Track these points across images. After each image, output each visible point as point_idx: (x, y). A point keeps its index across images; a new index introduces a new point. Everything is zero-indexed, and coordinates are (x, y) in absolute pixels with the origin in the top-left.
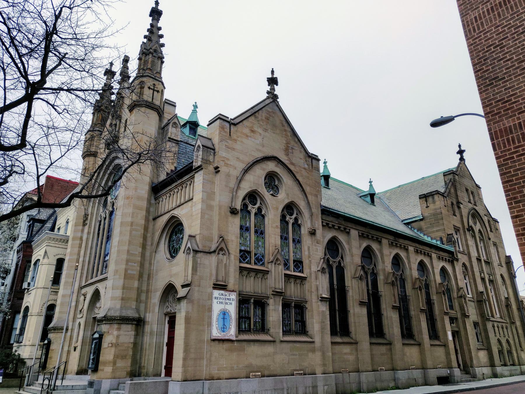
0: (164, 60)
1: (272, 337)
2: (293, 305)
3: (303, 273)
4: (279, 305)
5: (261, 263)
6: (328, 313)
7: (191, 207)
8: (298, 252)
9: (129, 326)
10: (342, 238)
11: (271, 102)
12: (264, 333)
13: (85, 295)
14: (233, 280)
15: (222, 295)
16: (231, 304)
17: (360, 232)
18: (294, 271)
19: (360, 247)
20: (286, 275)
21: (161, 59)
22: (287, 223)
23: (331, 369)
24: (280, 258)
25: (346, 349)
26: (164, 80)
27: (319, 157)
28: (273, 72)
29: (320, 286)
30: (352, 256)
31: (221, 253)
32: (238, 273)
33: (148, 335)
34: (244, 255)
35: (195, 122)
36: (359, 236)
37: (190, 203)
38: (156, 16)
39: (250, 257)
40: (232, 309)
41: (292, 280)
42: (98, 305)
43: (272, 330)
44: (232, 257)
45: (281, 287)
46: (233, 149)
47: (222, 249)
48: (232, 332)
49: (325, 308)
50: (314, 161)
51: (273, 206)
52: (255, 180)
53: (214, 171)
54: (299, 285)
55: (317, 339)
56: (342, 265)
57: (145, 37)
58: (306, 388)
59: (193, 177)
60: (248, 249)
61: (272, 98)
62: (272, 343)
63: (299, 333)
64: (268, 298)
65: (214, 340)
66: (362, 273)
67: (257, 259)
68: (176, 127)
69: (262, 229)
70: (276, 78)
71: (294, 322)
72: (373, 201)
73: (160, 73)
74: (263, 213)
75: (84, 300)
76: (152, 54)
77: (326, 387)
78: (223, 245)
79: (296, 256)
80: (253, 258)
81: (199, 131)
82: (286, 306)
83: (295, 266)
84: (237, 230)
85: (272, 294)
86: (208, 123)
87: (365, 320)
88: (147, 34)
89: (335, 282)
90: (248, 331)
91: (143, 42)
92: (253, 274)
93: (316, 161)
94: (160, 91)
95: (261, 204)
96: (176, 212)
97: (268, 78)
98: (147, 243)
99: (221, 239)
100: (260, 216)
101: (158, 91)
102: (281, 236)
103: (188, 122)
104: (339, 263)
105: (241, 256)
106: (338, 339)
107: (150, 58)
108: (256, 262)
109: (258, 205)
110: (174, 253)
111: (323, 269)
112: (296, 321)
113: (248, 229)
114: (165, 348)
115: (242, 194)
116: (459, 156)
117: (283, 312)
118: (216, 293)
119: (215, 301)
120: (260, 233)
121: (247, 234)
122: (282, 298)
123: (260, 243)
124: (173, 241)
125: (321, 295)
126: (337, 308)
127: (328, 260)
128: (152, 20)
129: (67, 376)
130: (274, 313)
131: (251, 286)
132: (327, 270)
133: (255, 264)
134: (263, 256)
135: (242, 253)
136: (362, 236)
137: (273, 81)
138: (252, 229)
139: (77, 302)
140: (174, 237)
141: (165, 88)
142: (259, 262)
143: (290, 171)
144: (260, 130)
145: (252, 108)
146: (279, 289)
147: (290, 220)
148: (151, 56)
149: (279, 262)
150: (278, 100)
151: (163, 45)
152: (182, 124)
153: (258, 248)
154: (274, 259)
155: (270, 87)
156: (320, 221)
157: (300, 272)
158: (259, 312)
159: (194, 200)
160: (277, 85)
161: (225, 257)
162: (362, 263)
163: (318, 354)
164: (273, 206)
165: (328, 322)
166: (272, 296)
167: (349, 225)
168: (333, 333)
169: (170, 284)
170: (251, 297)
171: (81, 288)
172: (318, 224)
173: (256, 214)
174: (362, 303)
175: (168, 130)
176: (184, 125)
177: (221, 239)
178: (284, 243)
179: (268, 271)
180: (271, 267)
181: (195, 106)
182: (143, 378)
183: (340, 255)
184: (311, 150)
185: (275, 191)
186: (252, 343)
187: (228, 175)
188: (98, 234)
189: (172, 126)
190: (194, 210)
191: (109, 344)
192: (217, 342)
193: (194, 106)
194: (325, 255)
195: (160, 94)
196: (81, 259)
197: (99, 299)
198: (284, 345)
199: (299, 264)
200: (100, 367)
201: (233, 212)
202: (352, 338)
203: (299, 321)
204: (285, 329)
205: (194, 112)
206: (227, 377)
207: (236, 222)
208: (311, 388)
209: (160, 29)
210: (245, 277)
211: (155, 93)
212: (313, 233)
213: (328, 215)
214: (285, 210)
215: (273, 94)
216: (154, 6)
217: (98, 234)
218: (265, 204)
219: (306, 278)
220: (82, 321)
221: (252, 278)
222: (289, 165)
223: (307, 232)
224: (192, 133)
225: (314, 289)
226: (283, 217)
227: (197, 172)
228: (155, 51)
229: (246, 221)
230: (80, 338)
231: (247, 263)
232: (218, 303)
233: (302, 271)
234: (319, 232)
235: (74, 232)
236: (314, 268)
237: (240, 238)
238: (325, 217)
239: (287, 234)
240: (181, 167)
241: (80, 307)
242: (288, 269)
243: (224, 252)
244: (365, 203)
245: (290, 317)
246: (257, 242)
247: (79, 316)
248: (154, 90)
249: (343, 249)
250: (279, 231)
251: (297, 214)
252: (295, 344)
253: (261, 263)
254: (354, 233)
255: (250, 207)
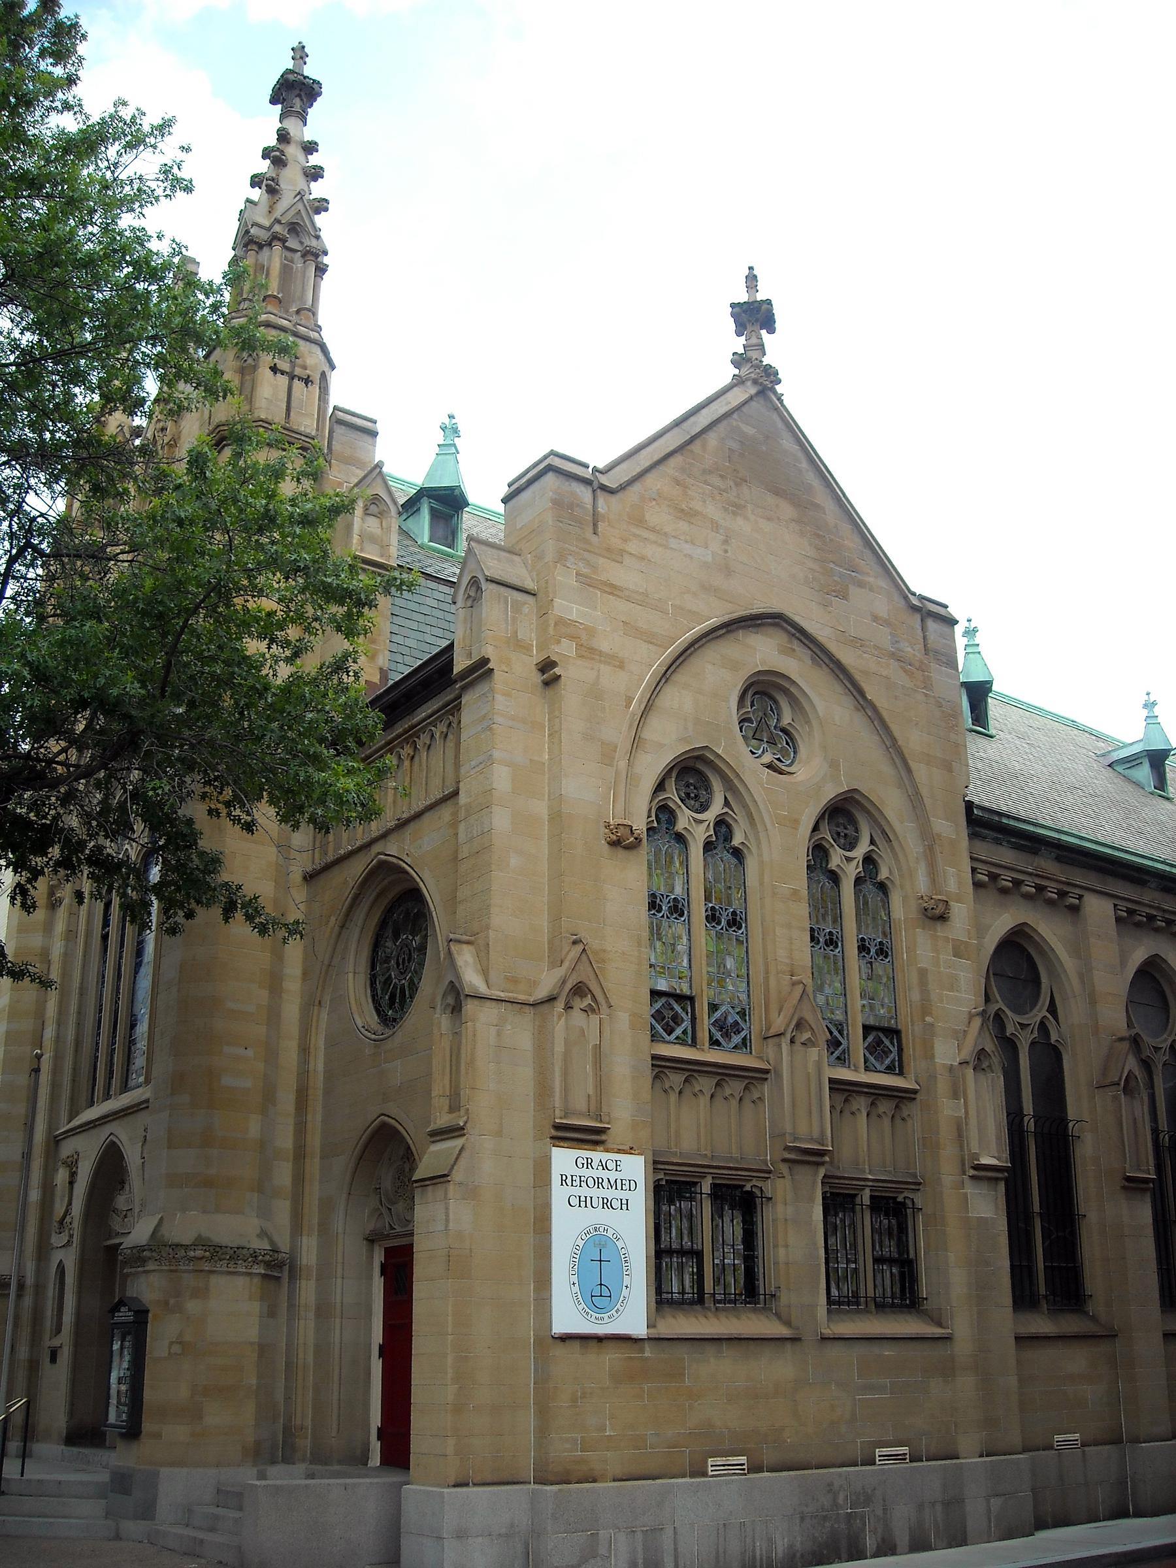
0: (326, 260)
1: (788, 1323)
2: (867, 1201)
3: (901, 1073)
4: (812, 1200)
5: (736, 1039)
6: (1002, 1225)
7: (454, 824)
8: (882, 992)
9: (240, 1283)
10: (1050, 930)
11: (751, 398)
12: (755, 1310)
13: (72, 1166)
14: (626, 1098)
15: (589, 1163)
16: (625, 1205)
17: (1123, 905)
18: (867, 1069)
19: (1123, 963)
20: (837, 1086)
21: (315, 257)
22: (835, 877)
23: (1015, 1437)
24: (809, 1016)
25: (1076, 1360)
26: (327, 336)
27: (954, 611)
28: (752, 280)
29: (973, 1121)
30: (1092, 1000)
31: (580, 1003)
32: (648, 1073)
33: (311, 1315)
34: (670, 1009)
35: (451, 489)
36: (1119, 920)
37: (446, 812)
38: (297, 101)
39: (693, 1019)
40: (632, 1228)
41: (861, 1104)
42: (121, 1202)
43: (784, 1298)
44: (623, 1020)
45: (816, 1135)
46: (612, 589)
47: (579, 990)
48: (632, 1316)
49: (987, 1207)
50: (931, 625)
51: (778, 809)
52: (706, 707)
53: (538, 678)
54: (887, 1121)
55: (962, 1327)
56: (1054, 1037)
57: (256, 181)
58: (921, 1507)
59: (454, 707)
60: (686, 990)
61: (755, 382)
62: (788, 1345)
63: (893, 1305)
64: (766, 1173)
65: (565, 1338)
66: (1132, 1064)
67: (720, 1025)
68: (380, 515)
69: (736, 905)
70: (769, 302)
71: (870, 1262)
72: (1161, 782)
73: (313, 311)
74: (736, 842)
75: (71, 1183)
76: (283, 241)
77: (996, 1503)
78: (584, 974)
79: (872, 1007)
80: (705, 1023)
81: (468, 522)
82: (838, 1202)
83: (871, 1049)
84: (640, 913)
85: (784, 1160)
86: (504, 490)
87: (1148, 1246)
88: (264, 166)
89: (1028, 1107)
90: (698, 1300)
91: (248, 201)
92: (706, 1084)
93: (945, 628)
94: (316, 377)
95: (727, 803)
96: (392, 848)
97: (733, 305)
98: (287, 971)
99: (580, 948)
100: (727, 856)
101: (307, 381)
102: (812, 930)
103: (423, 493)
104: (1043, 1027)
105: (658, 1016)
106: (1040, 1324)
107: (274, 258)
108: (718, 1035)
109: (716, 808)
110: (391, 1004)
111: (981, 1054)
112: (877, 1260)
113: (677, 909)
114: (377, 1366)
115: (652, 765)
116: (1145, 713)
117: (829, 1229)
118: (564, 1159)
119: (559, 1194)
120: (728, 921)
121: (679, 928)
122: (822, 1172)
123: (730, 963)
124: (387, 960)
125: (976, 1156)
126: (1036, 1208)
127: (998, 1018)
128: (283, 117)
129: (40, 1448)
130: (795, 1230)
131: (706, 1131)
132: (996, 1060)
133: (714, 1043)
134: (742, 1014)
135: (658, 1006)
136: (1130, 921)
137: (754, 316)
138: (693, 906)
139: (48, 1188)
140: (389, 944)
141: (333, 367)
142: (727, 1035)
143: (838, 670)
144: (712, 510)
145: (677, 423)
146: (812, 1140)
147: (847, 864)
148: (277, 248)
149: (806, 1035)
150: (779, 388)
151: (321, 206)
152: (402, 501)
153: (721, 983)
154: (788, 1025)
155: (742, 340)
156: (967, 866)
157: (890, 1070)
158: (733, 1228)
159: (463, 798)
160: (771, 330)
161: (594, 1018)
162: (1130, 1025)
163: (966, 1384)
164: (778, 809)
165: (1003, 1263)
166: (784, 1168)
167: (1080, 877)
168: (1024, 1299)
169: (384, 1125)
170: (702, 1170)
171: (55, 1142)
172: (957, 878)
173: (708, 846)
174: (1132, 1185)
175: (349, 527)
176: (411, 506)
177: (580, 948)
178: (826, 957)
179: (767, 1072)
180: (784, 1057)
181: (451, 430)
182: (300, 1468)
183: (1044, 1000)
184: (921, 580)
185: (782, 750)
186: (710, 1349)
187: (595, 693)
188: (105, 937)
189: (366, 509)
190: (462, 837)
191: (172, 1343)
192: (577, 1345)
193: (444, 428)
194: (987, 999)
195: (315, 389)
196: (49, 1033)
197: (123, 1182)
198: (835, 1352)
199: (885, 1039)
200: (147, 1426)
201: (621, 841)
202: (1094, 1319)
203: (890, 1261)
204: (834, 1292)
205: (448, 449)
206: (620, 1476)
207: (627, 883)
208: (939, 1508)
209: (310, 148)
210: (673, 1097)
211: (298, 385)
212: (936, 915)
213: (997, 842)
214: (671, 784)
215: (758, 365)
216: (290, 65)
217: (105, 937)
218: (745, 806)
219: (915, 1092)
220: (70, 1259)
221: (704, 1101)
222: (833, 647)
223: (914, 914)
224: (440, 533)
225: (946, 1133)
226: (819, 852)
227: (471, 684)
228: (294, 228)
229: (671, 876)
230: (68, 1317)
231: (680, 1041)
232: (574, 1201)
233: (897, 1068)
234: (961, 913)
235: (19, 931)
236: (946, 1053)
237: (652, 946)
238: (986, 851)
239: (835, 921)
240: (407, 671)
241: (59, 1209)
242: (842, 1060)
243: (588, 1000)
244: (1129, 788)
245: (854, 1245)
246: (716, 958)
247: (57, 1240)
248: (292, 377)
249: (1052, 973)
250: (802, 910)
251: (872, 842)
252: (876, 1349)
253: (736, 1039)
254: (1099, 910)
255: (684, 818)
